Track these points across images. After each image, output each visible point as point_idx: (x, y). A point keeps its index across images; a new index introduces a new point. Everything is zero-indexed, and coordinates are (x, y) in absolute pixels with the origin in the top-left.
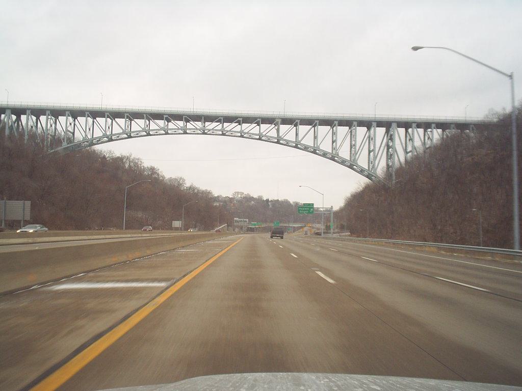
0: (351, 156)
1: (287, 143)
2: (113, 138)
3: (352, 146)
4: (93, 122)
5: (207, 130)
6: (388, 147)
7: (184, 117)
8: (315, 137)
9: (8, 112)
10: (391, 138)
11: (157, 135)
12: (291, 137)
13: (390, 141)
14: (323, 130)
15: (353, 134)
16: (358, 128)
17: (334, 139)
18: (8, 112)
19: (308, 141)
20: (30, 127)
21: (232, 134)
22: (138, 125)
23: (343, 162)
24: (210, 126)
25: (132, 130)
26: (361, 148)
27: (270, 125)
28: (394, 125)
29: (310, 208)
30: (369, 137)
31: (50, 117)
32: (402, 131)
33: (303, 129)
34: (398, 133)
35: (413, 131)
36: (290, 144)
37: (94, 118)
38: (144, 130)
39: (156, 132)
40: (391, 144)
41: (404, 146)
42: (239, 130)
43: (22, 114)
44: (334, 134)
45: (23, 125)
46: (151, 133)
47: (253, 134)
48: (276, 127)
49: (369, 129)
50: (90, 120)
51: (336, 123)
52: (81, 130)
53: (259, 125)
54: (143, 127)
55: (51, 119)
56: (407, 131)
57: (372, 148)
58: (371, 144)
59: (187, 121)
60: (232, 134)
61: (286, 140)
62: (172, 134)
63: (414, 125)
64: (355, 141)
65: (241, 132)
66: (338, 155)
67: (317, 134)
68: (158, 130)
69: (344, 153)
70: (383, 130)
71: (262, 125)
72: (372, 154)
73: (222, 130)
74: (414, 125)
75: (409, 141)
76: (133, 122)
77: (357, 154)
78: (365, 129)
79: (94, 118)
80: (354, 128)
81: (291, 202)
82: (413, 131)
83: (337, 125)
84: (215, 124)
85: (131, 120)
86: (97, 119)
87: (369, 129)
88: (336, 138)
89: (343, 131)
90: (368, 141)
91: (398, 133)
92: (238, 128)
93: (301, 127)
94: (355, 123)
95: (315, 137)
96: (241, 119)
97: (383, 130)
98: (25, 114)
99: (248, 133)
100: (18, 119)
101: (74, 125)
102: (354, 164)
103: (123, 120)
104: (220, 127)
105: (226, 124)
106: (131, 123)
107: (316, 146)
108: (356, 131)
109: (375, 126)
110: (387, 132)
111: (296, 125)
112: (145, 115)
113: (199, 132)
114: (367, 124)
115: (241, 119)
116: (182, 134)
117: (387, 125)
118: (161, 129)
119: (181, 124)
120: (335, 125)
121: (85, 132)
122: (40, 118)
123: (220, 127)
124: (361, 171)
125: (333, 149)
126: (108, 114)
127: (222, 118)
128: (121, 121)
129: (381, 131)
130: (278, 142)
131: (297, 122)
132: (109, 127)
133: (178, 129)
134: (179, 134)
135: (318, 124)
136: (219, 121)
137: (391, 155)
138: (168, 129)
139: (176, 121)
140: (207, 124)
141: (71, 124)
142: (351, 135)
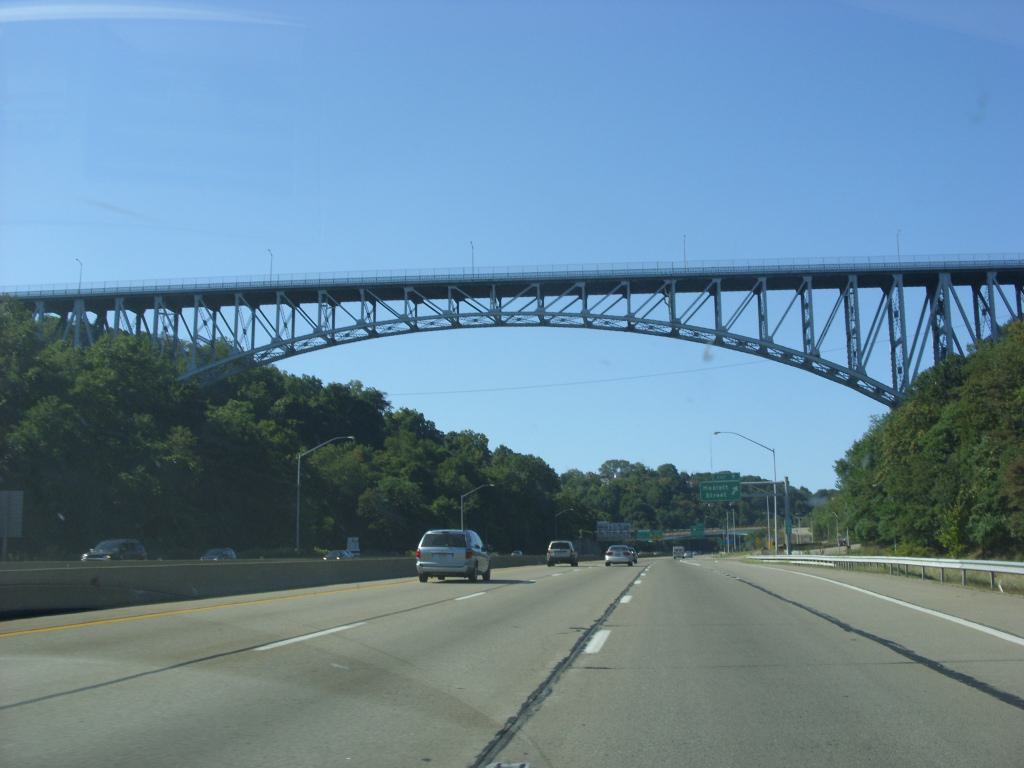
0: (849, 357)
1: (696, 334)
2: (336, 338)
3: (852, 334)
4: (254, 317)
5: (506, 314)
6: (937, 332)
7: (450, 288)
8: (762, 318)
9: (79, 305)
10: (941, 309)
11: (393, 334)
12: (704, 318)
13: (938, 317)
14: (779, 300)
15: (852, 303)
16: (861, 291)
17: (807, 317)
18: (79, 305)
19: (747, 327)
20: (160, 329)
21: (563, 320)
22: (349, 313)
23: (831, 372)
24: (555, 304)
25: (336, 327)
26: (870, 341)
27: (647, 296)
28: (945, 279)
29: (731, 485)
30: (889, 307)
31: (161, 311)
32: (965, 292)
33: (731, 299)
34: (956, 298)
35: (990, 292)
36: (808, 331)
37: (254, 306)
38: (361, 324)
39: (390, 328)
40: (941, 324)
41: (973, 327)
42: (624, 313)
43: (223, 305)
44: (806, 306)
45: (131, 323)
46: (419, 325)
47: (614, 318)
48: (667, 299)
49: (887, 292)
50: (246, 311)
51: (808, 279)
52: (234, 325)
53: (625, 296)
54: (359, 317)
55: (165, 314)
56: (976, 293)
57: (898, 335)
58: (895, 323)
59: (459, 298)
60: (563, 320)
61: (691, 328)
62: (468, 326)
63: (991, 276)
64: (857, 321)
65: (630, 317)
66: (818, 356)
67: (766, 311)
68: (395, 322)
69: (835, 351)
70: (921, 291)
71: (634, 297)
72: (899, 349)
73: (585, 314)
74: (991, 276)
75: (984, 314)
76: (338, 309)
77: (863, 354)
78: (878, 292)
79: (254, 306)
80: (851, 290)
81: (584, 473)
82: (990, 292)
83: (810, 285)
84: (566, 299)
85: (333, 305)
86: (261, 307)
87: (887, 292)
88: (811, 317)
89: (825, 299)
90: (887, 315)
91: (956, 298)
92: (620, 309)
93: (771, 294)
94: (898, 278)
95: (762, 318)
96: (582, 285)
97: (921, 291)
98: (190, 304)
99: (601, 316)
100: (102, 319)
101: (215, 326)
102: (860, 376)
103: (315, 306)
104: (578, 307)
105: (592, 299)
106: (333, 311)
107: (764, 336)
108: (856, 298)
109: (901, 282)
110: (931, 294)
111: (714, 292)
112: (362, 292)
113: (487, 320)
114: (881, 278)
115: (582, 285)
116: (491, 326)
117: (926, 278)
118: (403, 319)
119: (443, 304)
120: (805, 287)
121: (277, 331)
122: (145, 315)
123: (578, 307)
124: (878, 392)
125: (807, 342)
126: (325, 292)
127: (538, 285)
128: (311, 309)
129: (915, 296)
130: (674, 334)
131: (761, 283)
132: (285, 325)
133: (481, 314)
134: (486, 326)
135: (719, 286)
136: (577, 292)
137: (944, 350)
138: (458, 316)
139: (478, 300)
140: (548, 300)
141: (205, 323)
142: (846, 306)
